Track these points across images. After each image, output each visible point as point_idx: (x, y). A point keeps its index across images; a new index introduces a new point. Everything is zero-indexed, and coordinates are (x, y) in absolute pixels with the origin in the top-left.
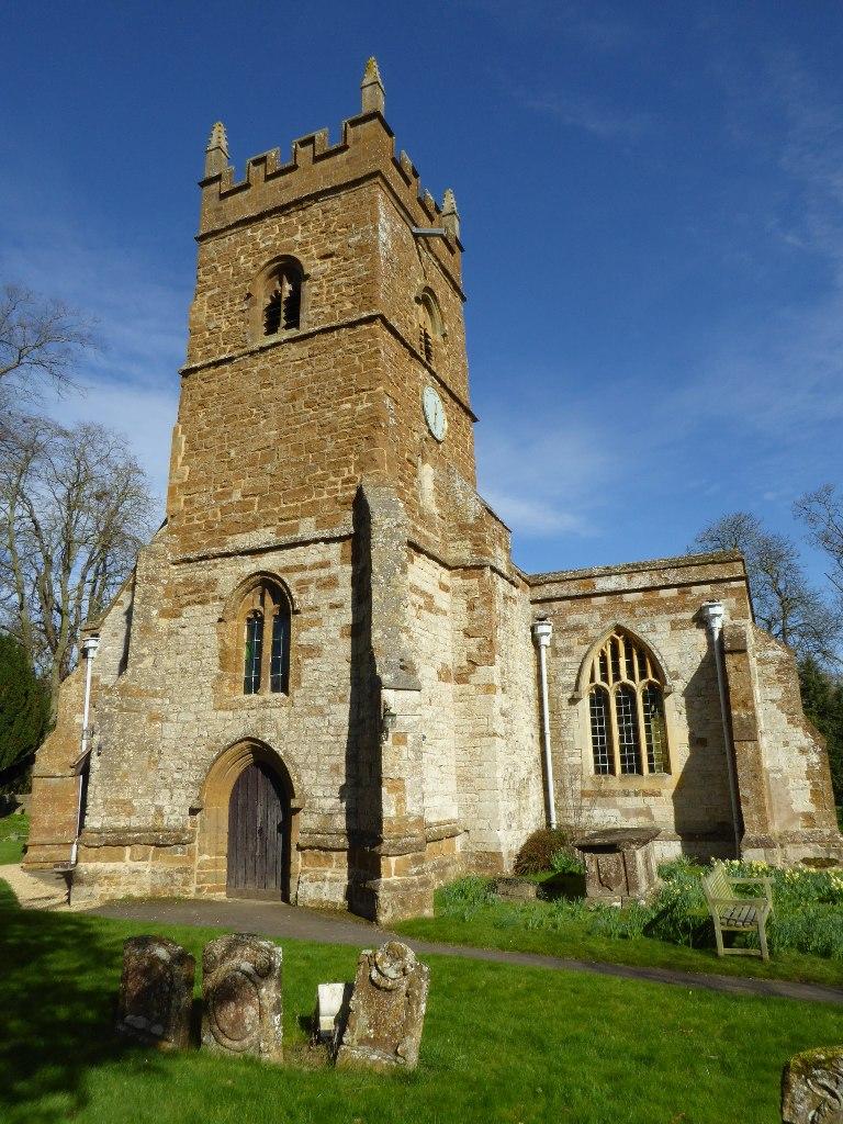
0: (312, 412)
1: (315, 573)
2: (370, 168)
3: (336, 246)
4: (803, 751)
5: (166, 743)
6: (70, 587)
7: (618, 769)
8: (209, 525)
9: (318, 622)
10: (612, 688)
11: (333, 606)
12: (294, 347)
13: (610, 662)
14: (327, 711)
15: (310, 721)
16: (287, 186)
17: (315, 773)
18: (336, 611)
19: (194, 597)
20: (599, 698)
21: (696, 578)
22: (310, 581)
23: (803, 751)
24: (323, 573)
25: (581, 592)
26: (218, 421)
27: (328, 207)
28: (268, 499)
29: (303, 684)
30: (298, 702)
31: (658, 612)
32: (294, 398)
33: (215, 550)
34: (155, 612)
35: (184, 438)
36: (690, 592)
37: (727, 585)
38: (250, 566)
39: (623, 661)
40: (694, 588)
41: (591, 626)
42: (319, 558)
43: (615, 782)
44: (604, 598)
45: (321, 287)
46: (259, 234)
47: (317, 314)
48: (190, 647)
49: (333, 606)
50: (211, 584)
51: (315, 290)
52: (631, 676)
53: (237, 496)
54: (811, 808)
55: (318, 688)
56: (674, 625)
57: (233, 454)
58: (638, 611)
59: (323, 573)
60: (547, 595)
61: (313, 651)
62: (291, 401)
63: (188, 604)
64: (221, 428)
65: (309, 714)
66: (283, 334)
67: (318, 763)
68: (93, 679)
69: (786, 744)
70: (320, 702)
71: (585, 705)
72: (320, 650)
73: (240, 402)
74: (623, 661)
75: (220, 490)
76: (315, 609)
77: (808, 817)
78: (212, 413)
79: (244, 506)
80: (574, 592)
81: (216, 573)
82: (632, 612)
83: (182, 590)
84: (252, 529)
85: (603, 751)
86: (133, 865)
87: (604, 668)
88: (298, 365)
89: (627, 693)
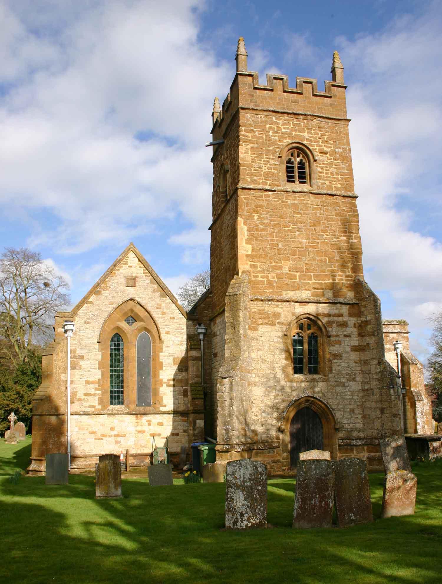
0: (325, 236)
1: (336, 319)
2: (285, 94)
3: (328, 150)
5: (256, 397)
11: (345, 336)
12: (312, 197)
14: (346, 384)
16: (296, 102)
17: (342, 413)
19: (265, 321)
21: (391, 330)
22: (333, 322)
24: (340, 319)
26: (268, 225)
27: (322, 125)
28: (305, 275)
29: (333, 372)
30: (332, 380)
35: (246, 228)
36: (389, 336)
37: (402, 334)
38: (300, 309)
42: (337, 312)
45: (322, 169)
47: (322, 184)
48: (266, 348)
49: (345, 336)
50: (277, 315)
53: (286, 270)
55: (342, 374)
57: (280, 246)
59: (340, 319)
62: (313, 226)
63: (262, 324)
64: (270, 229)
65: (338, 386)
67: (344, 408)
68: (71, 351)
70: (343, 380)
75: (273, 264)
76: (338, 336)
78: (264, 219)
83: (257, 316)
84: (297, 290)
86: (255, 459)
88: (315, 208)
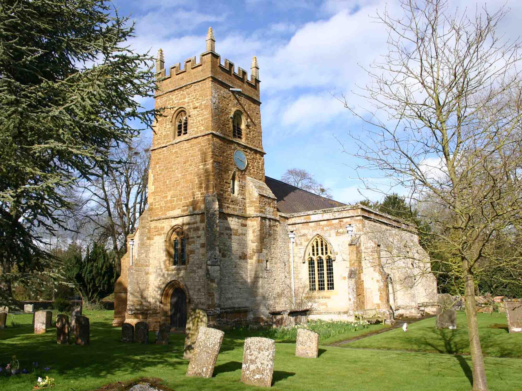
4: (378, 281)
6: (130, 206)
7: (326, 286)
8: (161, 207)
9: (194, 242)
10: (315, 258)
13: (315, 248)
15: (191, 275)
16: (182, 78)
18: (199, 239)
19: (157, 233)
20: (311, 262)
23: (378, 281)
25: (305, 221)
31: (331, 229)
32: (185, 163)
33: (163, 217)
34: (145, 238)
36: (343, 221)
39: (320, 248)
40: (344, 220)
41: (309, 234)
43: (316, 293)
44: (313, 223)
46: (174, 97)
51: (192, 121)
52: (322, 254)
54: (379, 302)
56: (338, 233)
58: (325, 229)
60: (294, 222)
61: (192, 252)
66: (183, 137)
69: (373, 279)
70: (195, 268)
71: (307, 263)
72: (194, 251)
73: (169, 163)
74: (320, 248)
76: (193, 238)
77: (378, 305)
79: (171, 201)
80: (302, 221)
81: (163, 225)
82: (323, 229)
85: (331, 280)
87: (313, 250)
89: (320, 262)
